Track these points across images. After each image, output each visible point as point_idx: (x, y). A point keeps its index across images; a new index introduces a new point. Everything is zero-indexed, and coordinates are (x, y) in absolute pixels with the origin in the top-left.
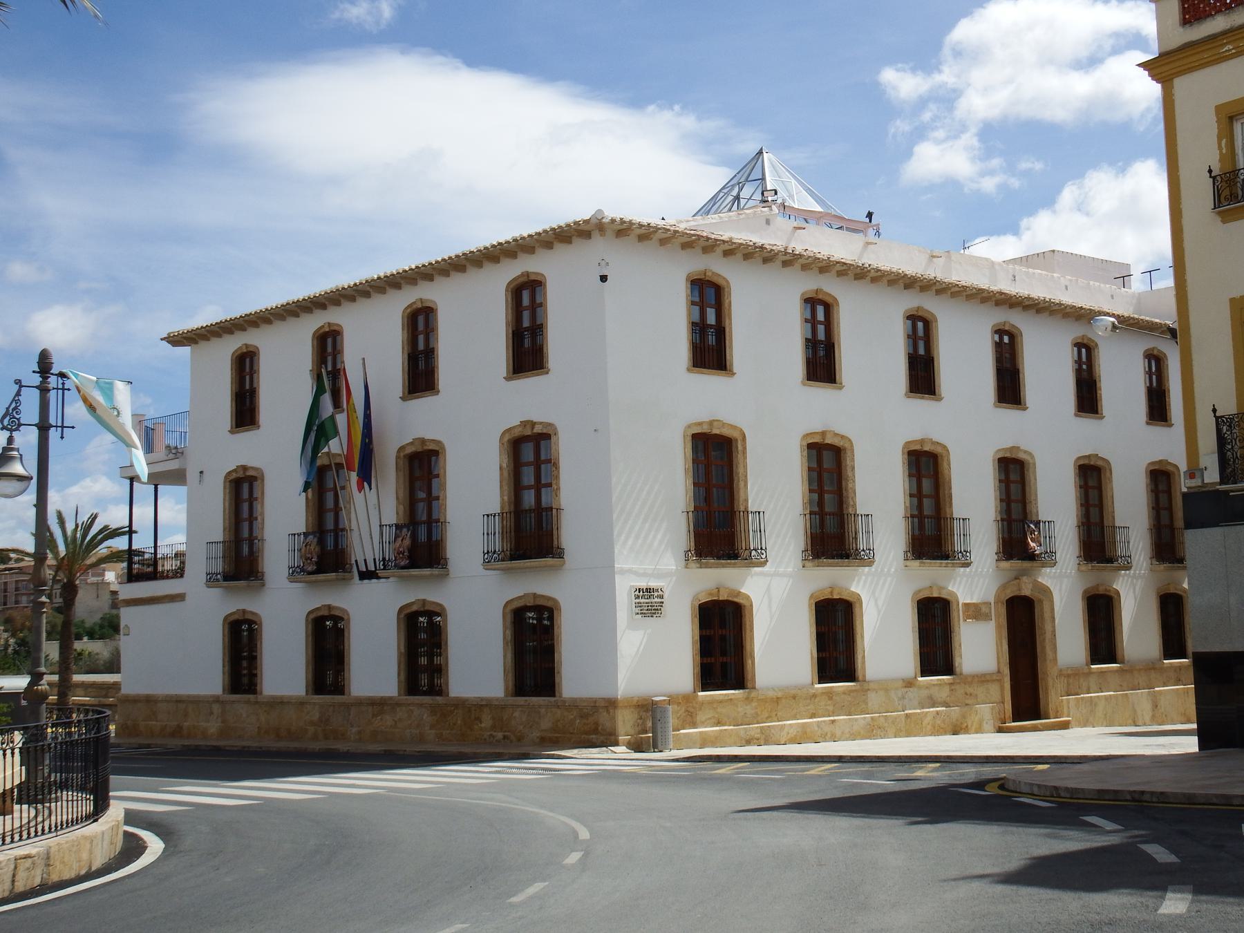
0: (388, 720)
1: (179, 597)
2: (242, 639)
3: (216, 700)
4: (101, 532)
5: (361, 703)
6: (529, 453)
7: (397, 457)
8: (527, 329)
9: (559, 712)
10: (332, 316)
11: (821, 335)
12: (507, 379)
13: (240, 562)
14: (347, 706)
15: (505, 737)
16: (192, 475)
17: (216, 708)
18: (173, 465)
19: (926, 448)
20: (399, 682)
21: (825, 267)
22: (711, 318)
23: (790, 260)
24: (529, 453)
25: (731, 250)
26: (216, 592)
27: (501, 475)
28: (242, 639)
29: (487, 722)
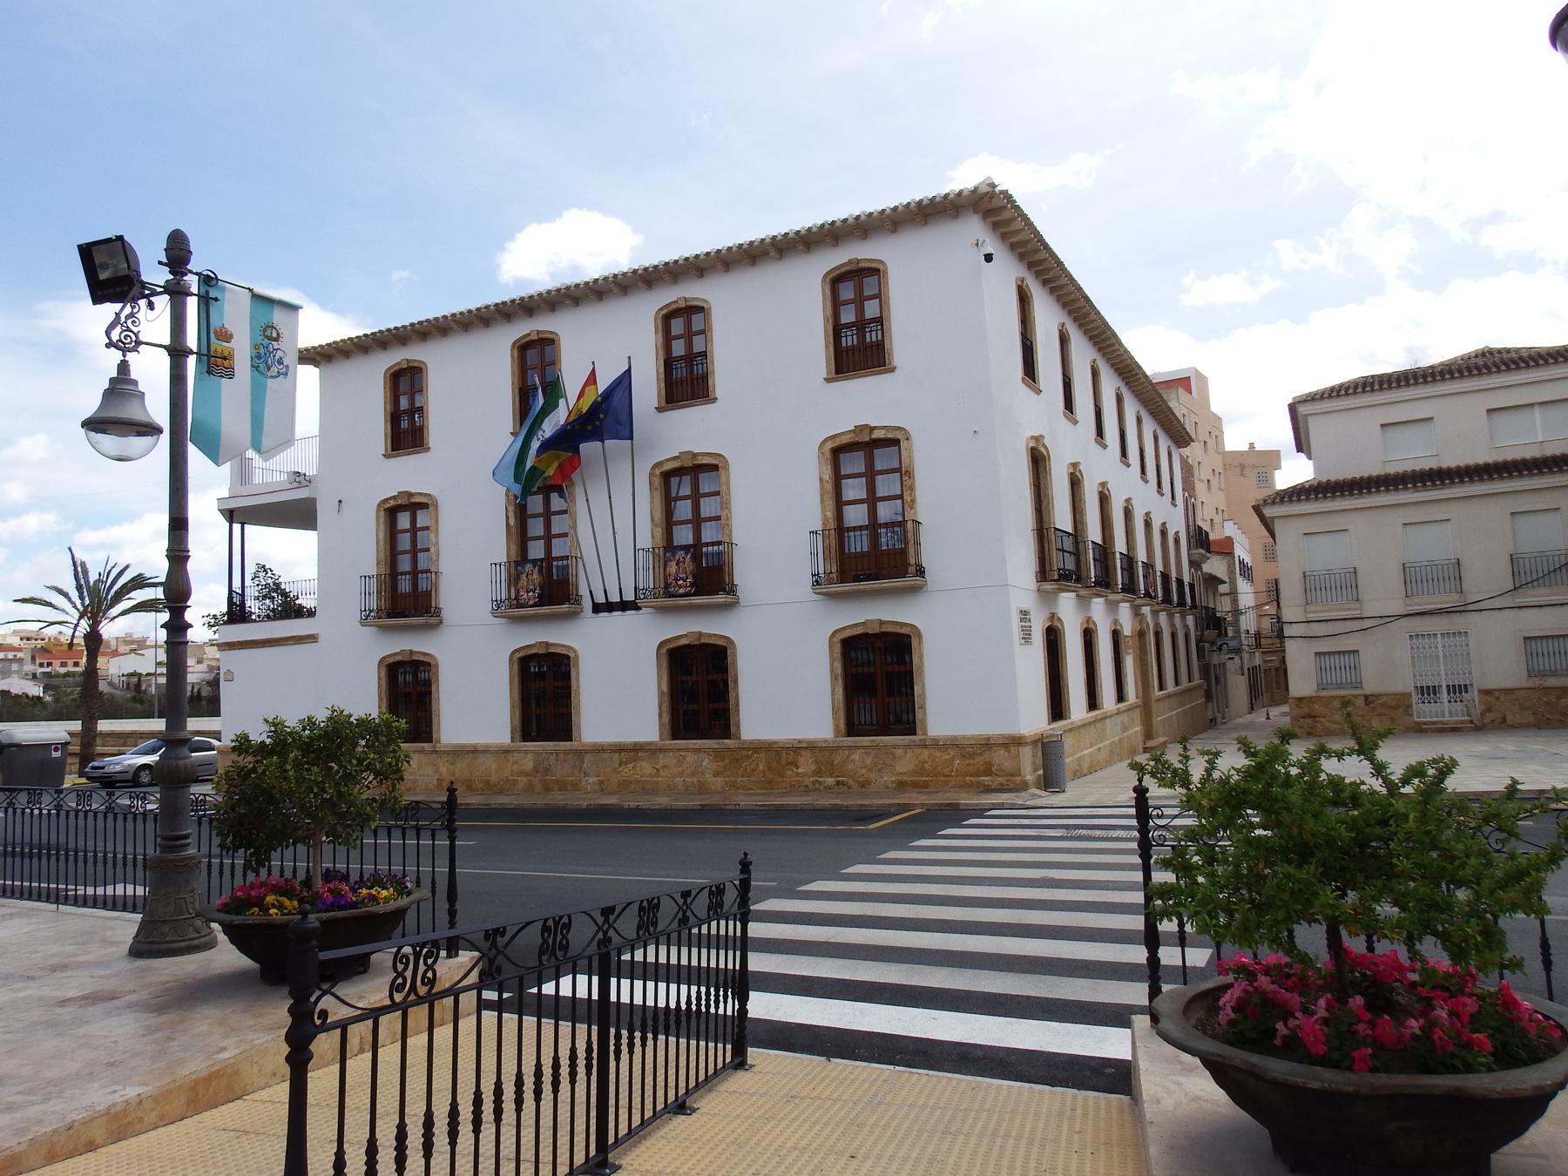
1: (312, 638)
4: (133, 579)
6: (865, 456)
7: (651, 475)
8: (405, 412)
9: (926, 753)
10: (691, 291)
12: (386, 456)
13: (405, 596)
14: (580, 753)
15: (838, 783)
16: (324, 512)
20: (661, 725)
24: (865, 456)
26: (369, 631)
27: (822, 488)
29: (806, 765)
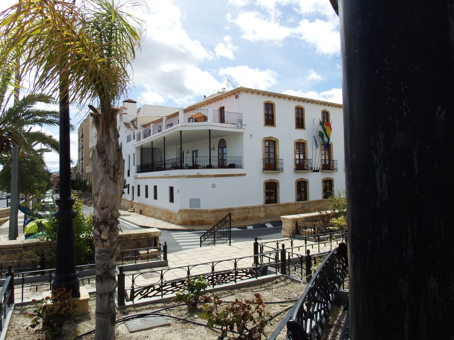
0: (321, 205)
1: (155, 187)
2: (271, 190)
3: (263, 206)
5: (314, 202)
11: (300, 117)
14: (310, 203)
17: (262, 209)
18: (215, 143)
19: (301, 141)
21: (300, 99)
22: (270, 113)
23: (291, 98)
25: (280, 96)
28: (271, 190)
